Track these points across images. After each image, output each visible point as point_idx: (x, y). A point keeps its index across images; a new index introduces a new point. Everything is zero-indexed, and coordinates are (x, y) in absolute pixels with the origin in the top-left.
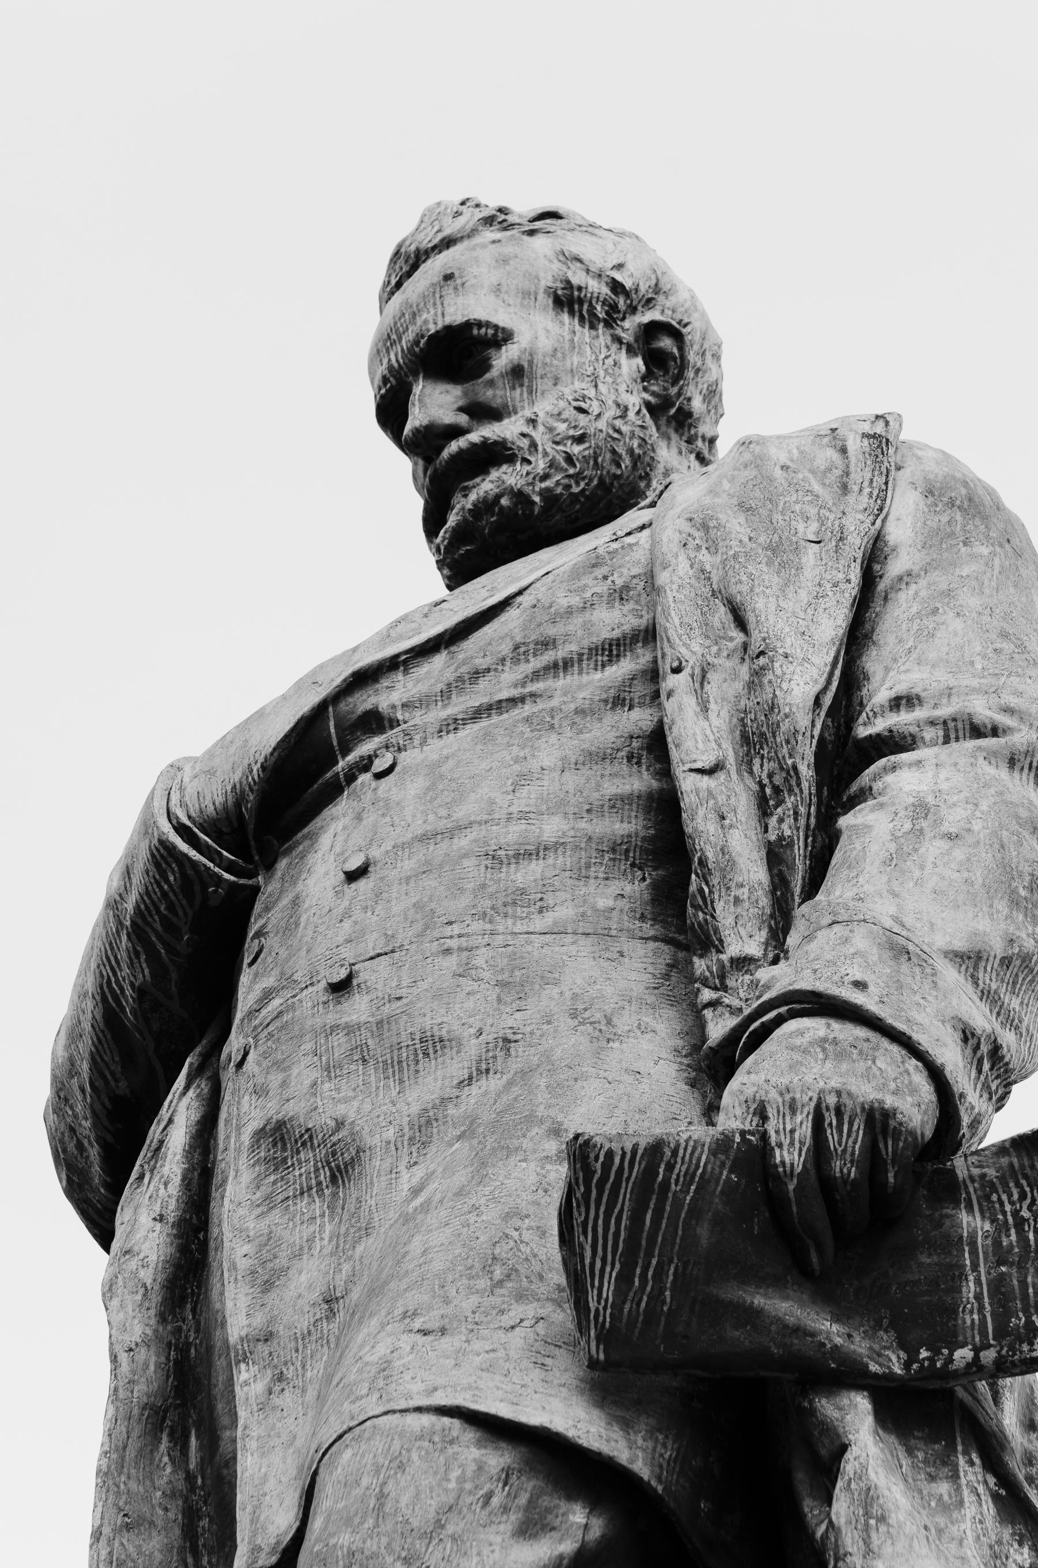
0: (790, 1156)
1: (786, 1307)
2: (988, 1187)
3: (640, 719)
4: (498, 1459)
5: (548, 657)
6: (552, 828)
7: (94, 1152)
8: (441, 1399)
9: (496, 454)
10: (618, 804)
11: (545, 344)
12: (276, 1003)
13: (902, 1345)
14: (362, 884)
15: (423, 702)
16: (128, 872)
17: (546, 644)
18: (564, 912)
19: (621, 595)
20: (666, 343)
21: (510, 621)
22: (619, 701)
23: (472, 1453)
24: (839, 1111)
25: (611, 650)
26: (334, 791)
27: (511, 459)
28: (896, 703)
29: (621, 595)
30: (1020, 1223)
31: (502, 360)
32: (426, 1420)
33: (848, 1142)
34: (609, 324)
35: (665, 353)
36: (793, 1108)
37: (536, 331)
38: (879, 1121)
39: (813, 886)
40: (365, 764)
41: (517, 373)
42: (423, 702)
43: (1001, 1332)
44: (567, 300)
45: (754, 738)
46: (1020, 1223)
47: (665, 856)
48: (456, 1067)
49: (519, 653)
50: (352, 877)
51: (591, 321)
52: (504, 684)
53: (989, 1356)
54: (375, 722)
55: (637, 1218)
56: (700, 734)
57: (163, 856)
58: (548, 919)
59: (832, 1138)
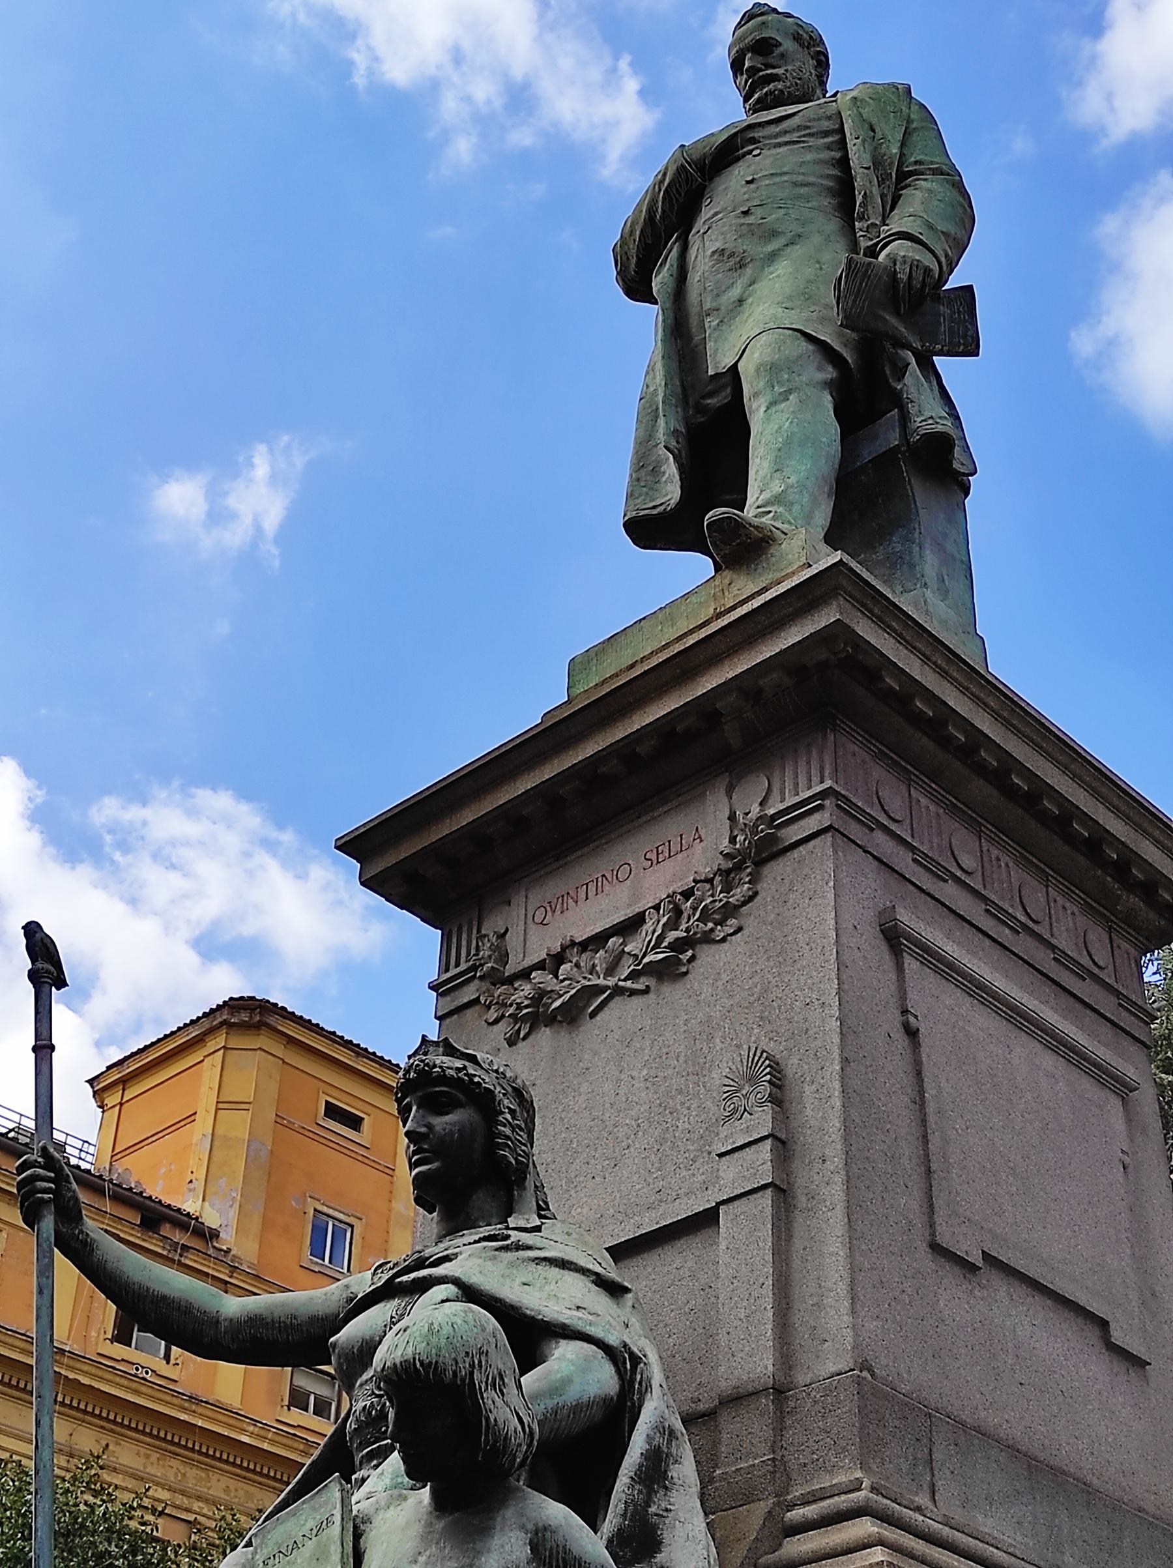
2: (950, 301)
3: (838, 155)
4: (811, 347)
5: (808, 131)
6: (811, 179)
7: (634, 261)
8: (794, 326)
10: (829, 176)
12: (720, 216)
14: (752, 186)
16: (665, 175)
17: (808, 127)
18: (814, 204)
19: (829, 118)
20: (823, 58)
21: (796, 121)
22: (829, 147)
25: (826, 134)
28: (916, 163)
29: (829, 118)
30: (959, 312)
33: (919, 276)
35: (822, 62)
36: (905, 262)
37: (788, 45)
38: (928, 271)
39: (892, 209)
41: (782, 55)
43: (950, 342)
44: (797, 38)
45: (877, 162)
46: (959, 312)
49: (799, 128)
50: (748, 182)
51: (802, 45)
52: (794, 137)
53: (946, 348)
54: (753, 141)
55: (861, 284)
56: (858, 156)
57: (681, 170)
58: (810, 205)
59: (914, 273)
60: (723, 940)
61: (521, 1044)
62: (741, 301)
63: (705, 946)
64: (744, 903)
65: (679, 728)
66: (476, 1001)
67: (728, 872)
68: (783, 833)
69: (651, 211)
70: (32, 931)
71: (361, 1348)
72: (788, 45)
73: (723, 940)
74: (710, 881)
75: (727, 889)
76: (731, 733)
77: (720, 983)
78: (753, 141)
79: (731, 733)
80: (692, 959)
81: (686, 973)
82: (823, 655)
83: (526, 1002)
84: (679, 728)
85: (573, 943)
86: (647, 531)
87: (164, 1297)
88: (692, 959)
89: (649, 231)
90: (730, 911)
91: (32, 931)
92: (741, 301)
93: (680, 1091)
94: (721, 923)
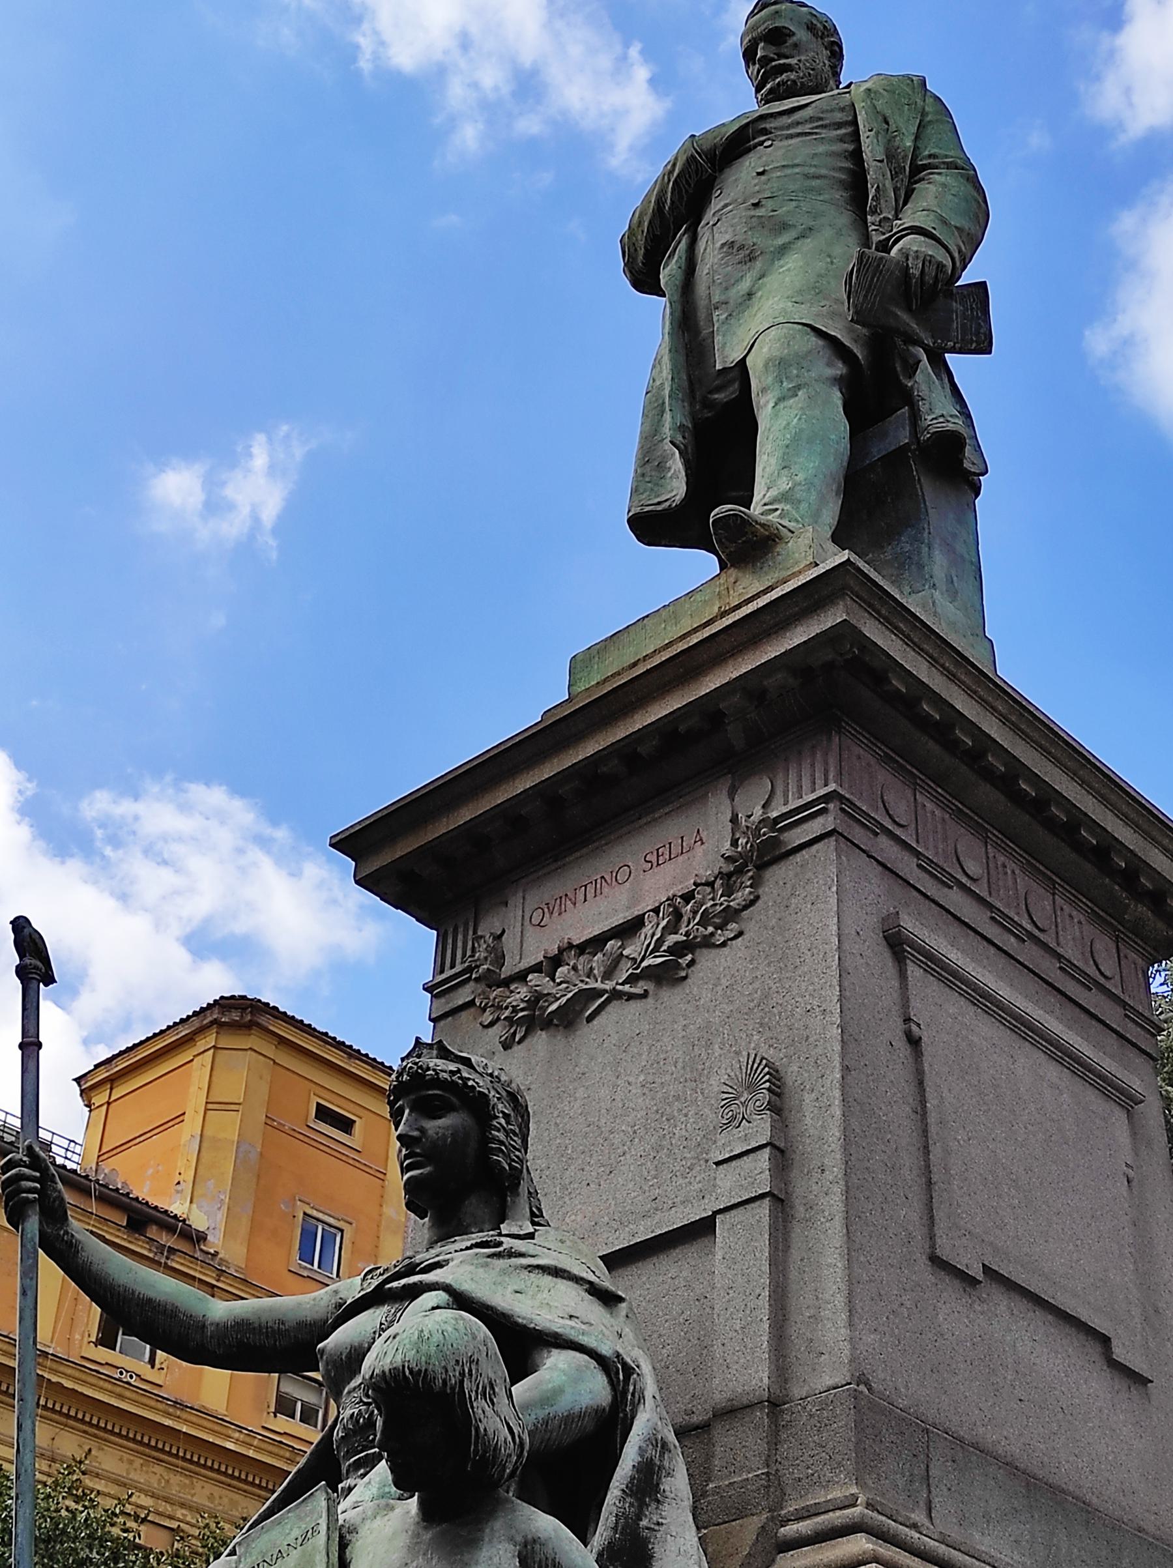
0: (915, 272)
1: (904, 316)
3: (851, 147)
4: (821, 342)
5: (820, 123)
6: (823, 172)
7: (642, 252)
9: (787, 68)
11: (804, 39)
12: (730, 208)
13: (933, 337)
15: (782, 128)
17: (821, 119)
19: (842, 109)
20: (837, 48)
21: (808, 112)
22: (841, 139)
23: (814, 341)
24: (930, 262)
25: (839, 125)
26: (749, 150)
27: (792, 71)
28: (930, 156)
29: (842, 109)
30: (972, 309)
31: (791, 41)
32: (800, 327)
33: (931, 271)
34: (822, 38)
35: (836, 53)
36: (917, 257)
37: (802, 35)
38: (940, 266)
40: (761, 144)
42: (782, 128)
43: (962, 340)
45: (891, 155)
46: (972, 309)
47: (856, 185)
48: (793, 234)
49: (811, 119)
50: (759, 174)
51: (815, 35)
52: (807, 128)
54: (765, 132)
55: (872, 279)
56: (871, 149)
57: (691, 160)
59: (926, 269)
60: (724, 944)
62: (750, 295)
63: (705, 951)
64: (745, 908)
65: (682, 728)
68: (786, 836)
69: (660, 202)
70: (20, 926)
72: (802, 35)
73: (724, 944)
74: (711, 884)
75: (728, 893)
76: (734, 733)
78: (765, 132)
80: (692, 963)
81: (685, 978)
82: (828, 655)
84: (682, 728)
85: (571, 946)
86: (652, 527)
88: (692, 963)
89: (657, 222)
91: (20, 926)
92: (750, 295)
94: (721, 927)
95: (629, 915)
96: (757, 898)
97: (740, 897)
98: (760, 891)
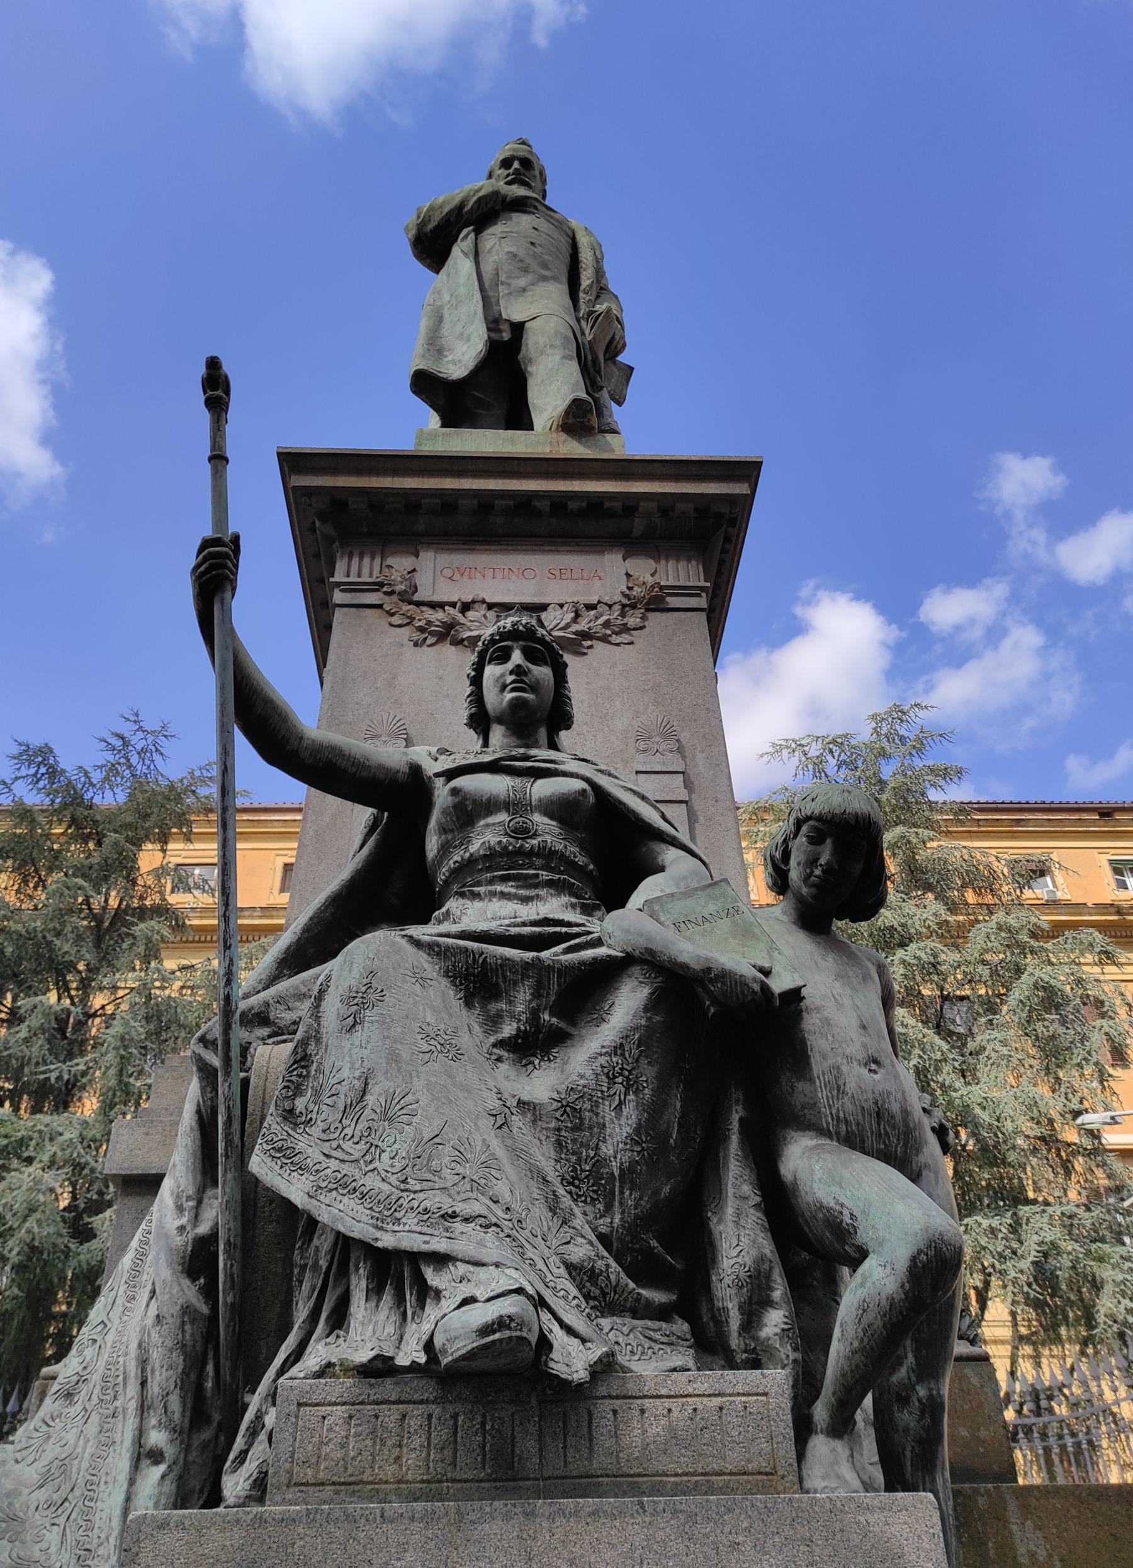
60: (618, 645)
61: (425, 648)
62: (524, 290)
63: (601, 644)
64: (635, 629)
65: (607, 505)
66: (380, 606)
67: (624, 606)
68: (668, 599)
69: (462, 205)
70: (213, 364)
71: (489, 800)
72: (537, 173)
73: (618, 645)
74: (610, 606)
75: (623, 615)
76: (638, 525)
77: (617, 670)
78: (536, 208)
79: (638, 525)
80: (591, 647)
81: (585, 654)
82: (724, 509)
83: (438, 623)
84: (607, 505)
85: (483, 601)
86: (425, 384)
87: (272, 701)
88: (591, 647)
89: (455, 212)
90: (626, 629)
91: (213, 364)
92: (524, 290)
93: (586, 724)
94: (617, 634)
95: (536, 600)
96: (644, 627)
97: (632, 620)
98: (646, 623)
